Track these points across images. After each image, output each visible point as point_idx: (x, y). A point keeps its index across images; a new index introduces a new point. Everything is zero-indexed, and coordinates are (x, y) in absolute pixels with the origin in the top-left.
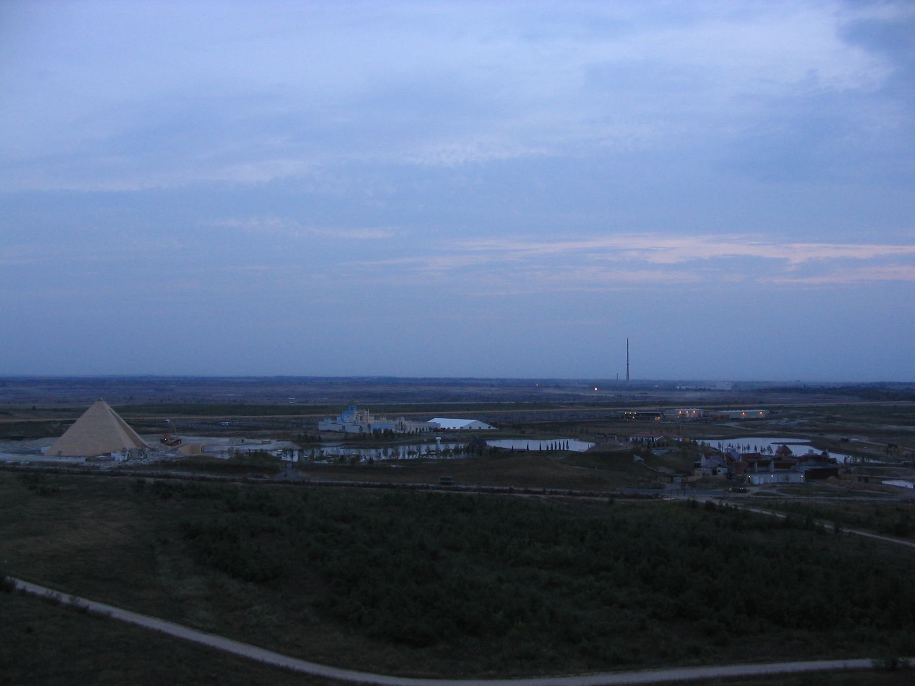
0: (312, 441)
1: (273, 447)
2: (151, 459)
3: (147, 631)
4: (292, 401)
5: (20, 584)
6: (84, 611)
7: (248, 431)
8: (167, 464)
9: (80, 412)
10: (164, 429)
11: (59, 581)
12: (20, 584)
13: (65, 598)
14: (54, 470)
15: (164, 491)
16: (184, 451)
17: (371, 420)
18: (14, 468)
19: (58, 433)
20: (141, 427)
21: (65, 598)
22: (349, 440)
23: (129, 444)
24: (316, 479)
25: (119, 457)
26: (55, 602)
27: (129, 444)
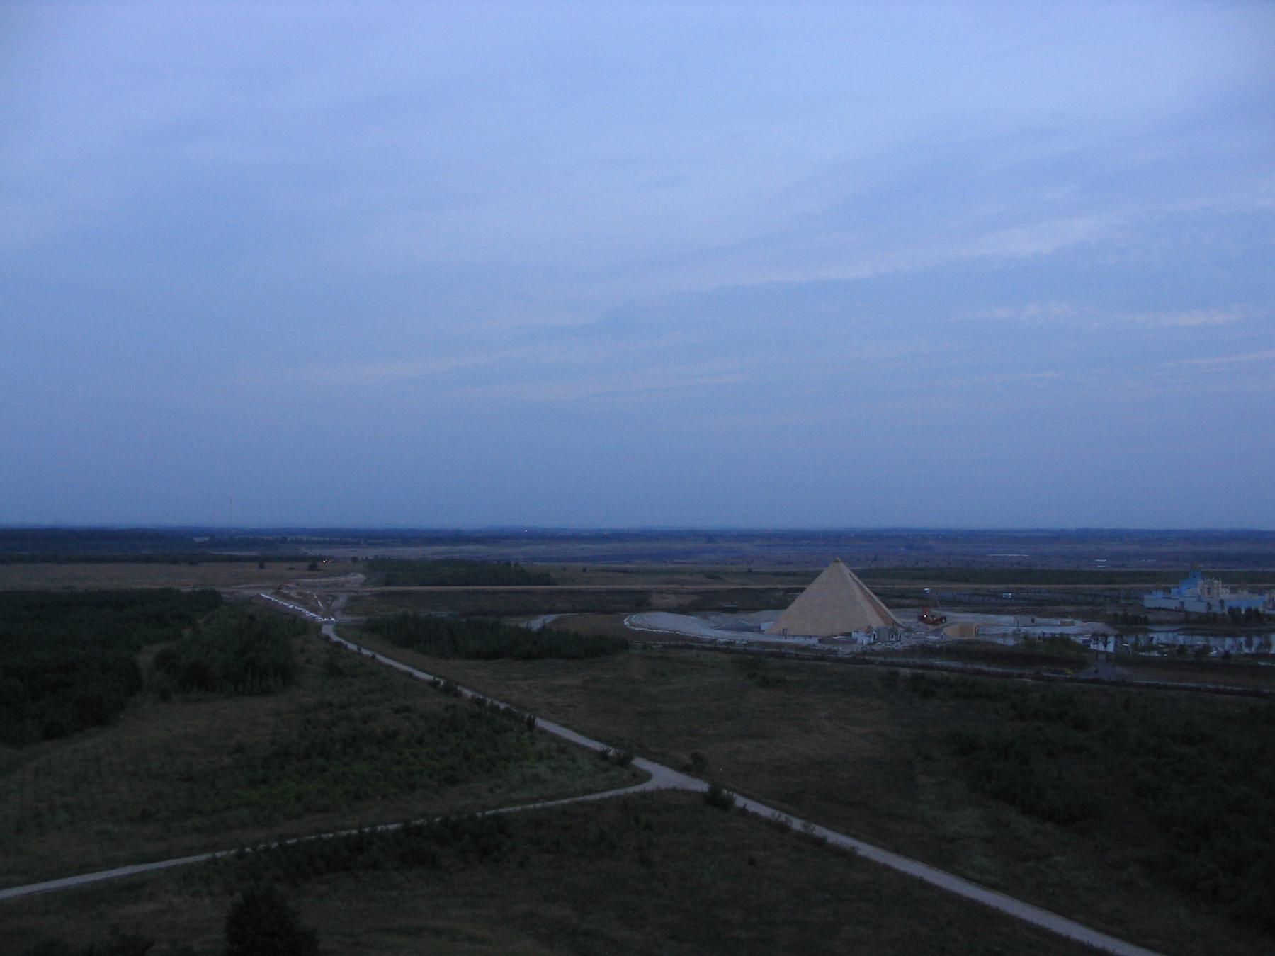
0: (1134, 622)
1: (1077, 629)
2: (905, 642)
3: (902, 876)
4: (1102, 565)
5: (740, 801)
6: (821, 842)
7: (1037, 606)
8: (927, 650)
9: (811, 577)
10: (923, 601)
11: (790, 800)
12: (740, 801)
13: (797, 824)
14: (778, 653)
15: (924, 687)
16: (950, 633)
17: (1225, 594)
18: (728, 648)
19: (783, 605)
20: (891, 599)
21: (797, 824)
22: (1191, 622)
23: (876, 622)
24: (1141, 679)
25: (863, 639)
26: (783, 828)
27: (876, 622)
